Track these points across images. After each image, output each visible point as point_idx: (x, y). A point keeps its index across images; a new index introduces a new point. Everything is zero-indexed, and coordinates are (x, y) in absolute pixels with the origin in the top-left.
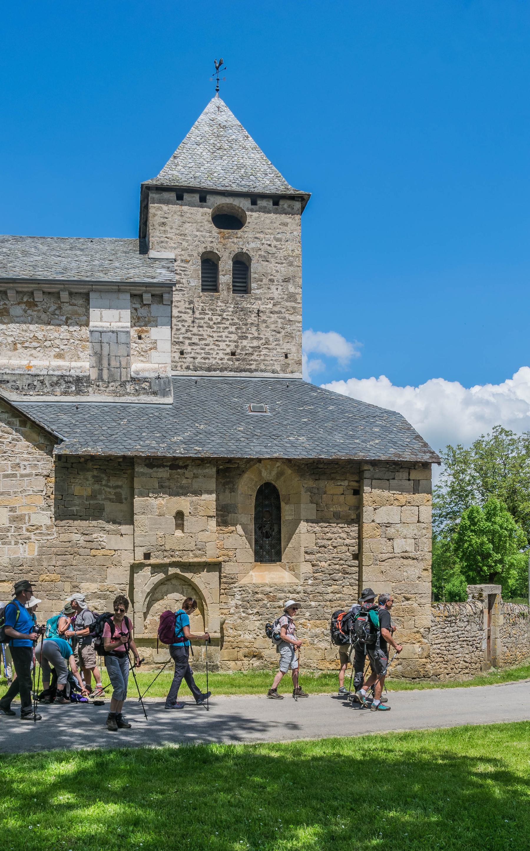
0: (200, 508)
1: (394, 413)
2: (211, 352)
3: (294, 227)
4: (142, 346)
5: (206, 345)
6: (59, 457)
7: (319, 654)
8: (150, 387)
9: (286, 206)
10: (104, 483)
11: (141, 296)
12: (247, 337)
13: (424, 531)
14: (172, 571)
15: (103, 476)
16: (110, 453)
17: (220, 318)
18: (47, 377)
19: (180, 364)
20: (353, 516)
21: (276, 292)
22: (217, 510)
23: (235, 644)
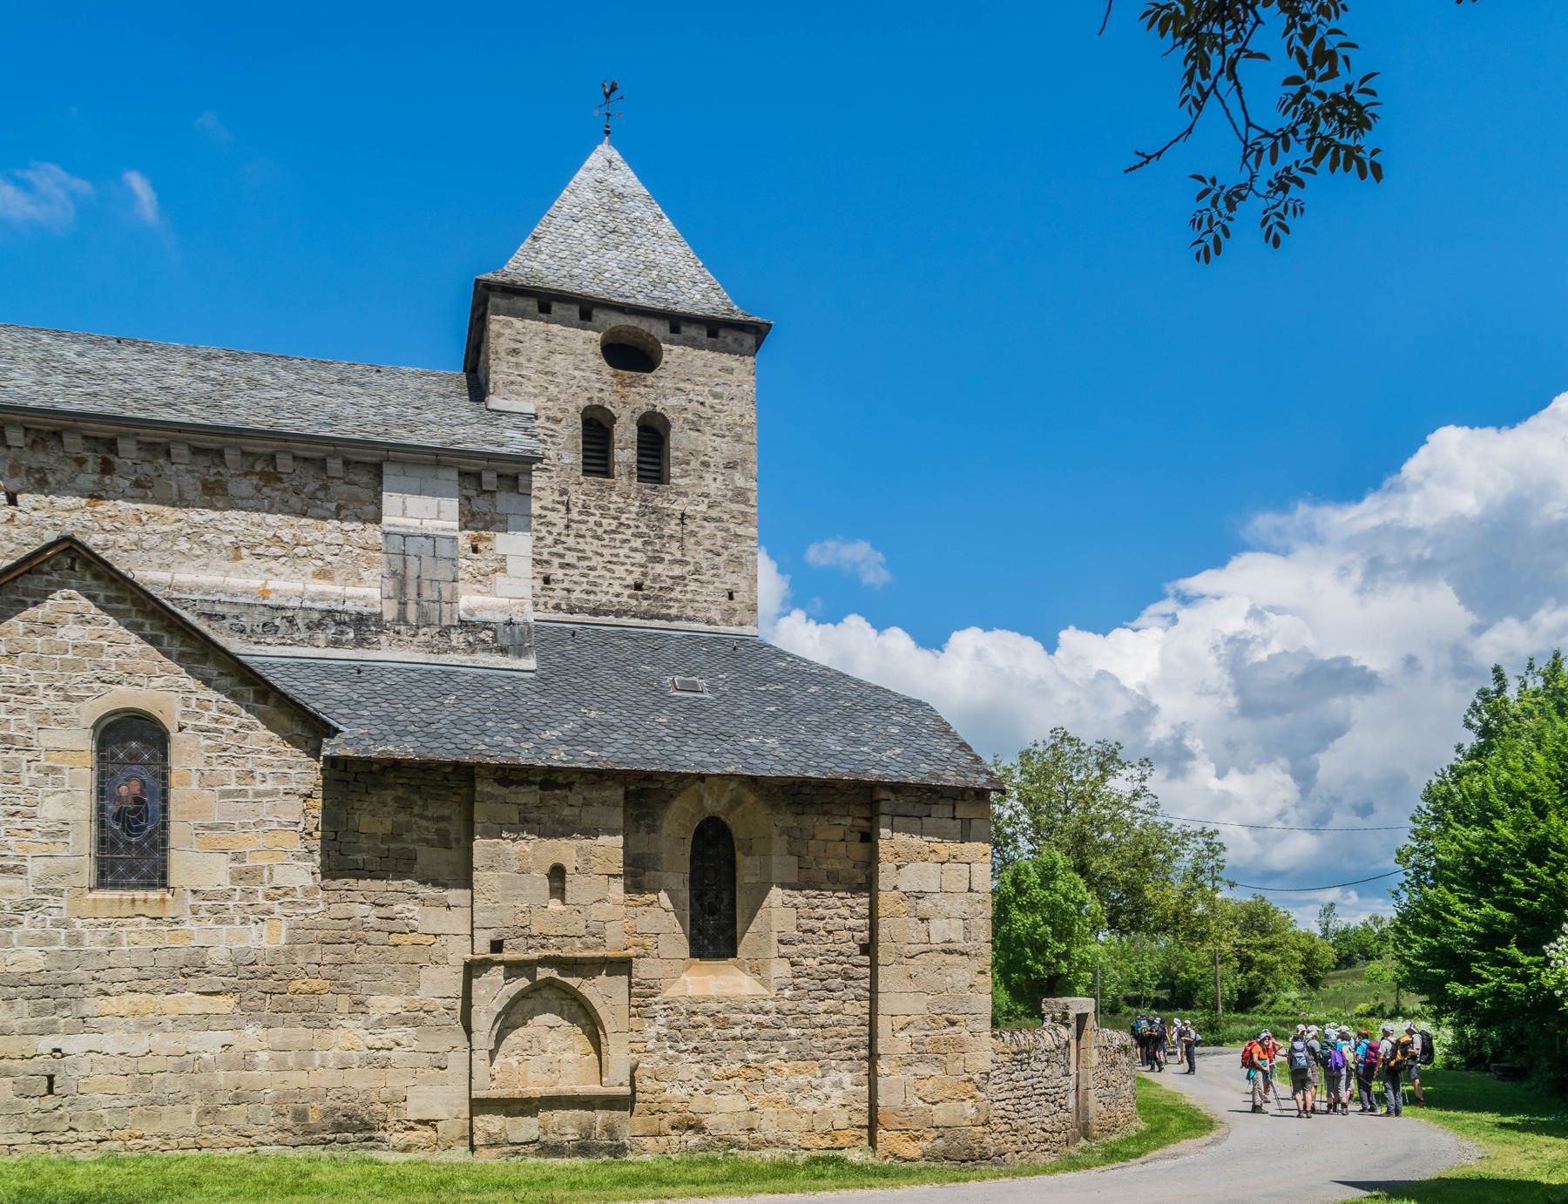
0: (595, 861)
1: (919, 704)
2: (599, 581)
3: (743, 376)
4: (480, 564)
5: (591, 569)
6: (332, 762)
7: (803, 1121)
8: (495, 639)
9: (729, 340)
10: (416, 810)
11: (478, 476)
12: (662, 560)
13: (979, 907)
14: (543, 973)
15: (416, 797)
16: (430, 756)
17: (615, 523)
18: (301, 613)
19: (542, 600)
20: (861, 879)
21: (713, 485)
22: (625, 864)
23: (655, 1106)
